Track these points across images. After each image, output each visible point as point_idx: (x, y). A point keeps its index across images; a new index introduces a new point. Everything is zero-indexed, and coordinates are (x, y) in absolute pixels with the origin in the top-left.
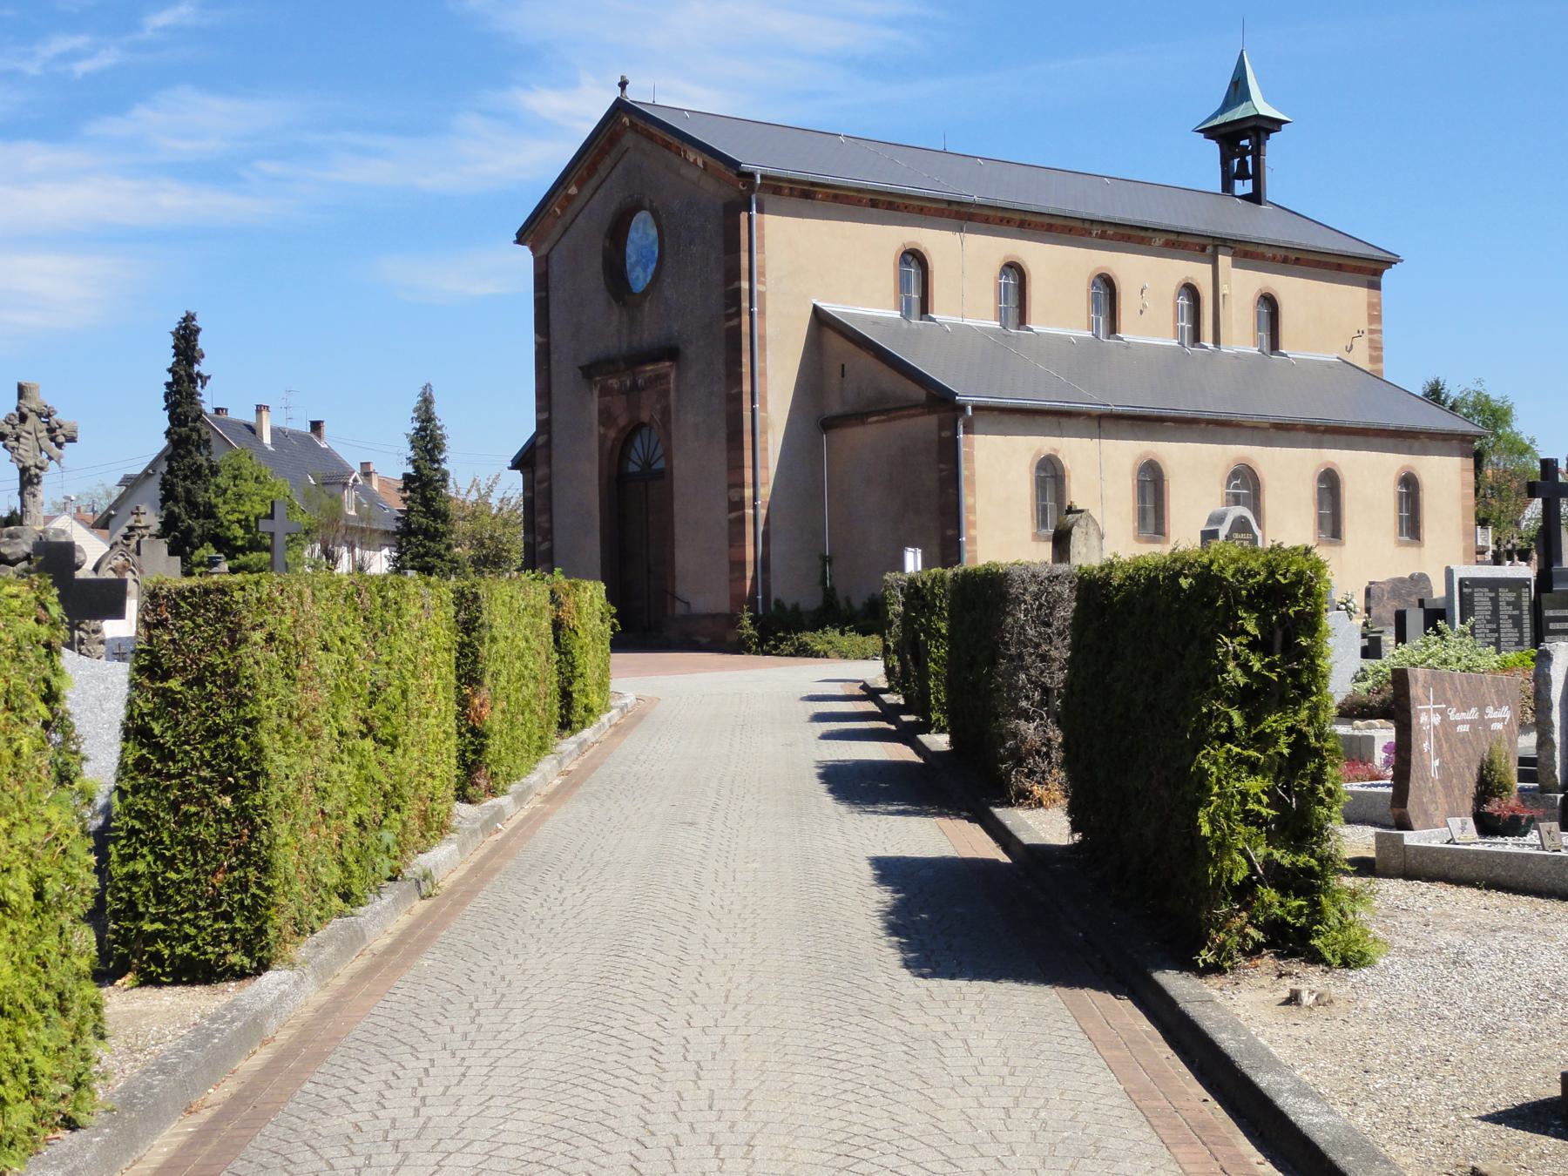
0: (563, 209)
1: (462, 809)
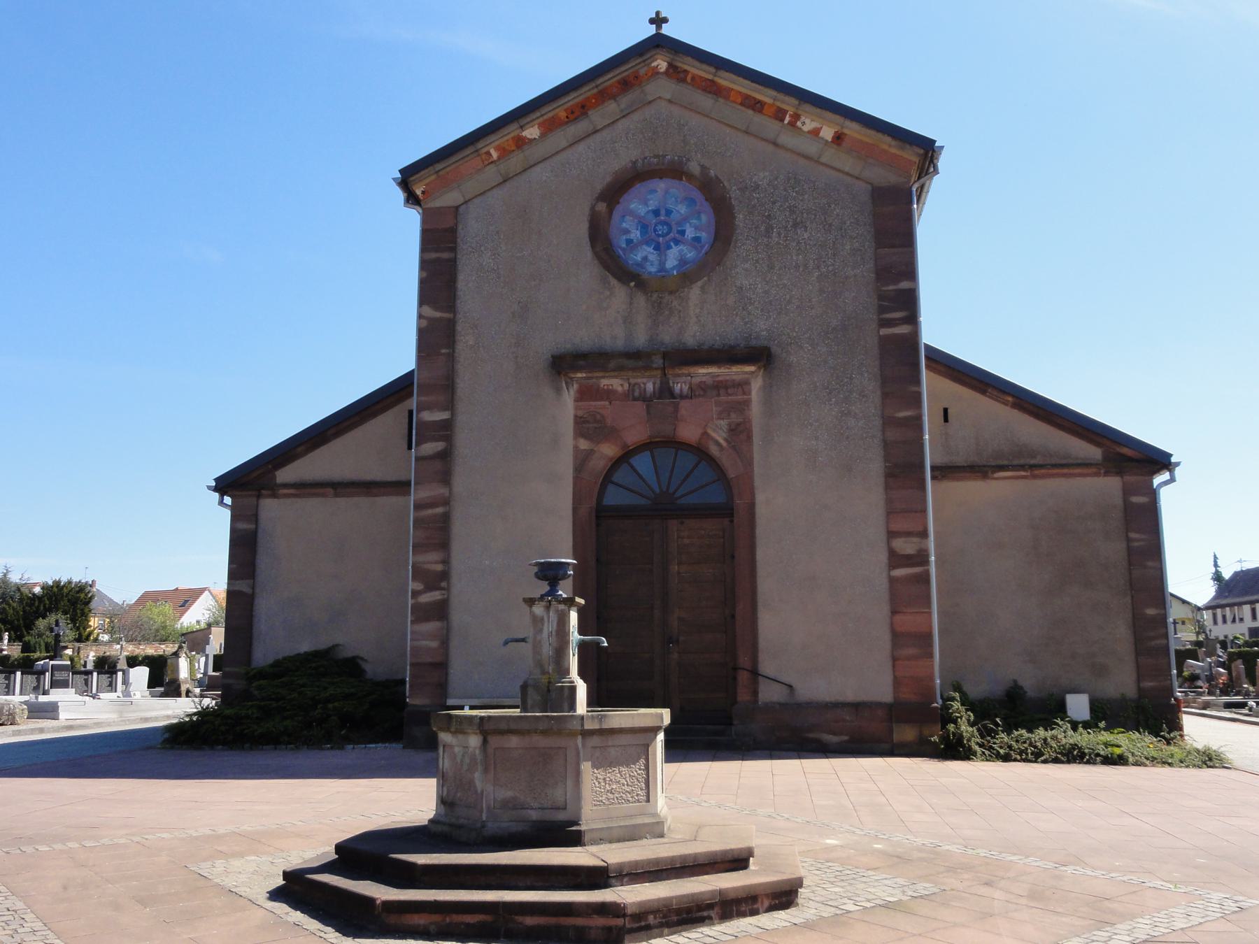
0: (504, 153)
1: (63, 715)
